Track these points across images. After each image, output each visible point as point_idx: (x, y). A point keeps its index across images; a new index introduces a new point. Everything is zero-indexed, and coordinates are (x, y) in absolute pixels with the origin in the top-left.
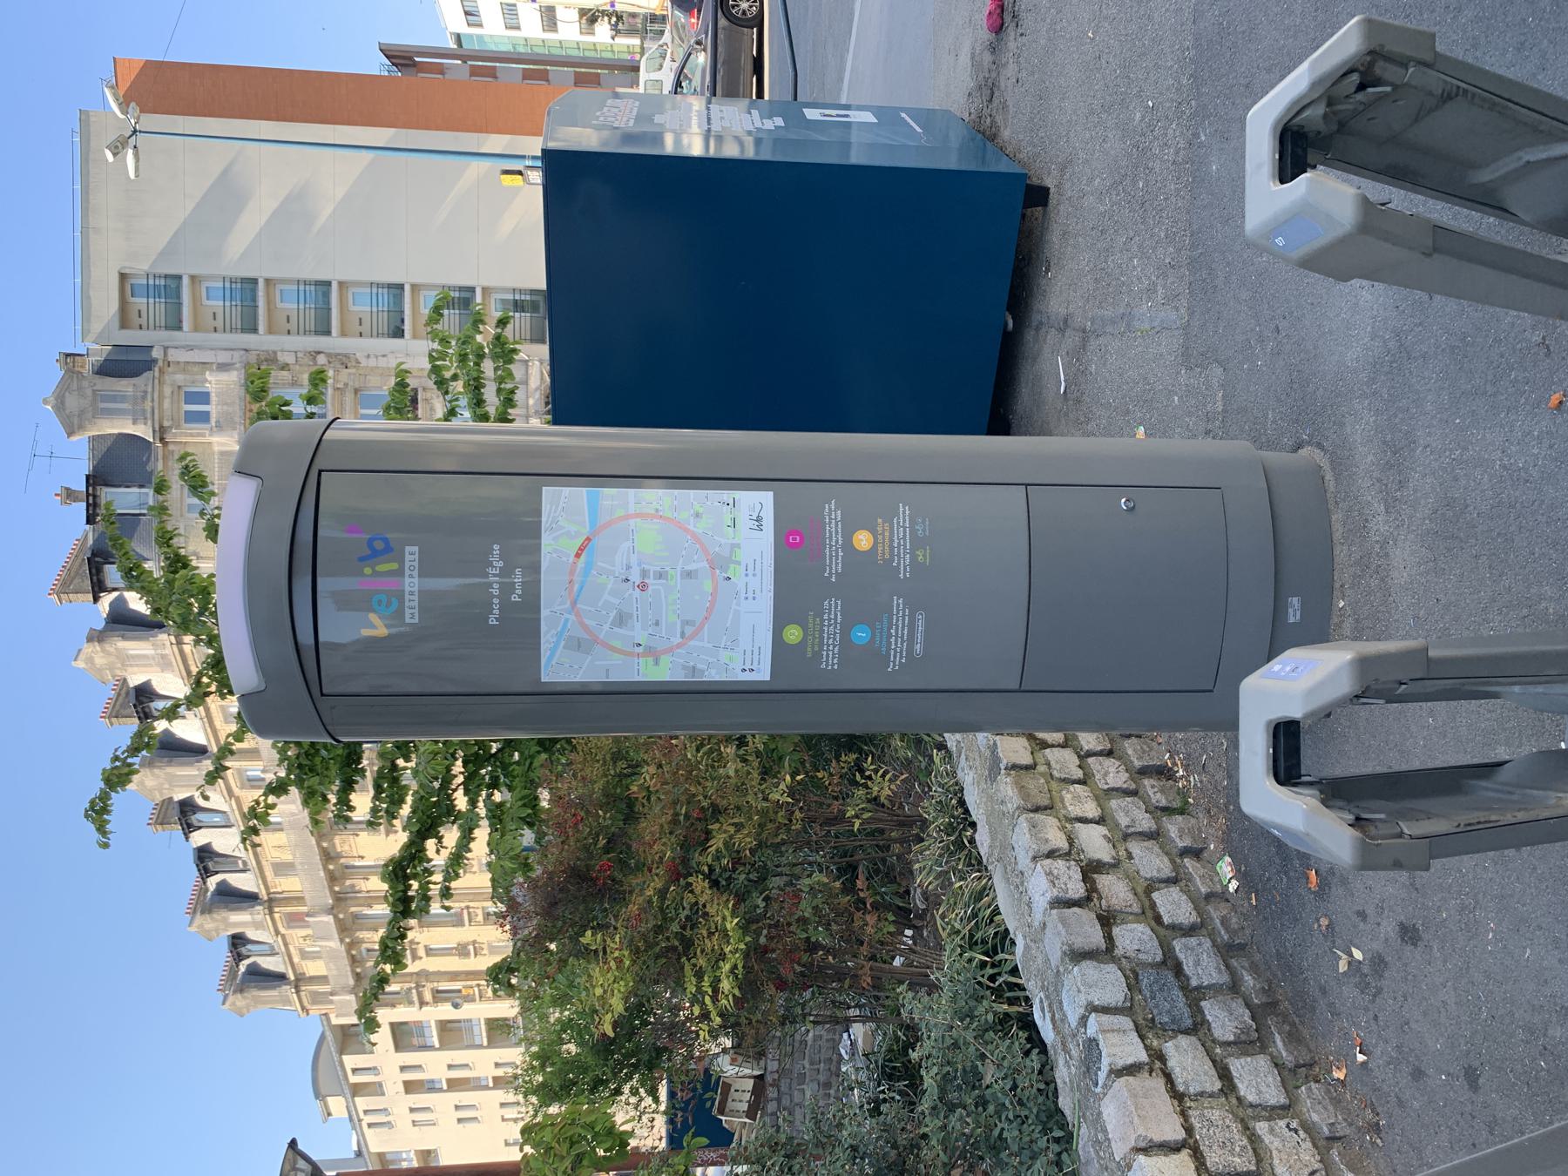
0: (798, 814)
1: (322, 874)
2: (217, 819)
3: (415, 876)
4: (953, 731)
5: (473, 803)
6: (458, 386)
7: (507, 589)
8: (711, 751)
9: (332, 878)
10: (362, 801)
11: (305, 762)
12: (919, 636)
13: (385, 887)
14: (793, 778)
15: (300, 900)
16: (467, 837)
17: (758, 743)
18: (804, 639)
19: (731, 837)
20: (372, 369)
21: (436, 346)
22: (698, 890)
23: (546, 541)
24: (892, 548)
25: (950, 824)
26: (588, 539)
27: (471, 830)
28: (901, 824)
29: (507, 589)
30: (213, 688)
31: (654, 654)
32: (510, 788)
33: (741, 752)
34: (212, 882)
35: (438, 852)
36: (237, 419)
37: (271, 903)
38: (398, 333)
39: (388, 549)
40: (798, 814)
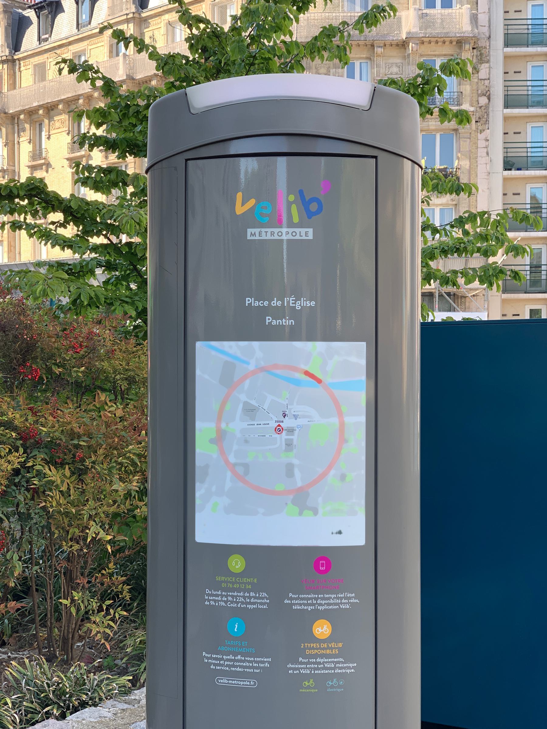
0: (76, 547)
1: (35, 104)
2: (84, 17)
3: (31, 203)
4: (148, 697)
5: (95, 248)
6: (457, 233)
7: (279, 313)
8: (134, 464)
9: (31, 113)
10: (98, 158)
11: (131, 110)
12: (234, 682)
13: (23, 180)
14: (109, 542)
15: (13, 86)
16: (65, 244)
17: (142, 511)
18: (231, 574)
19: (57, 486)
20: (476, 143)
21: (493, 217)
22: (11, 458)
23: (319, 346)
24: (316, 656)
25: (64, 693)
26: (319, 381)
27: (70, 247)
28: (65, 640)
29: (279, 313)
30: (195, 31)
31: (220, 438)
32: (106, 283)
33: (133, 493)
34: (31, 14)
35: (53, 223)
36: (429, 30)
37: (11, 62)
38: (508, 165)
39: (310, 214)
40: (76, 547)
